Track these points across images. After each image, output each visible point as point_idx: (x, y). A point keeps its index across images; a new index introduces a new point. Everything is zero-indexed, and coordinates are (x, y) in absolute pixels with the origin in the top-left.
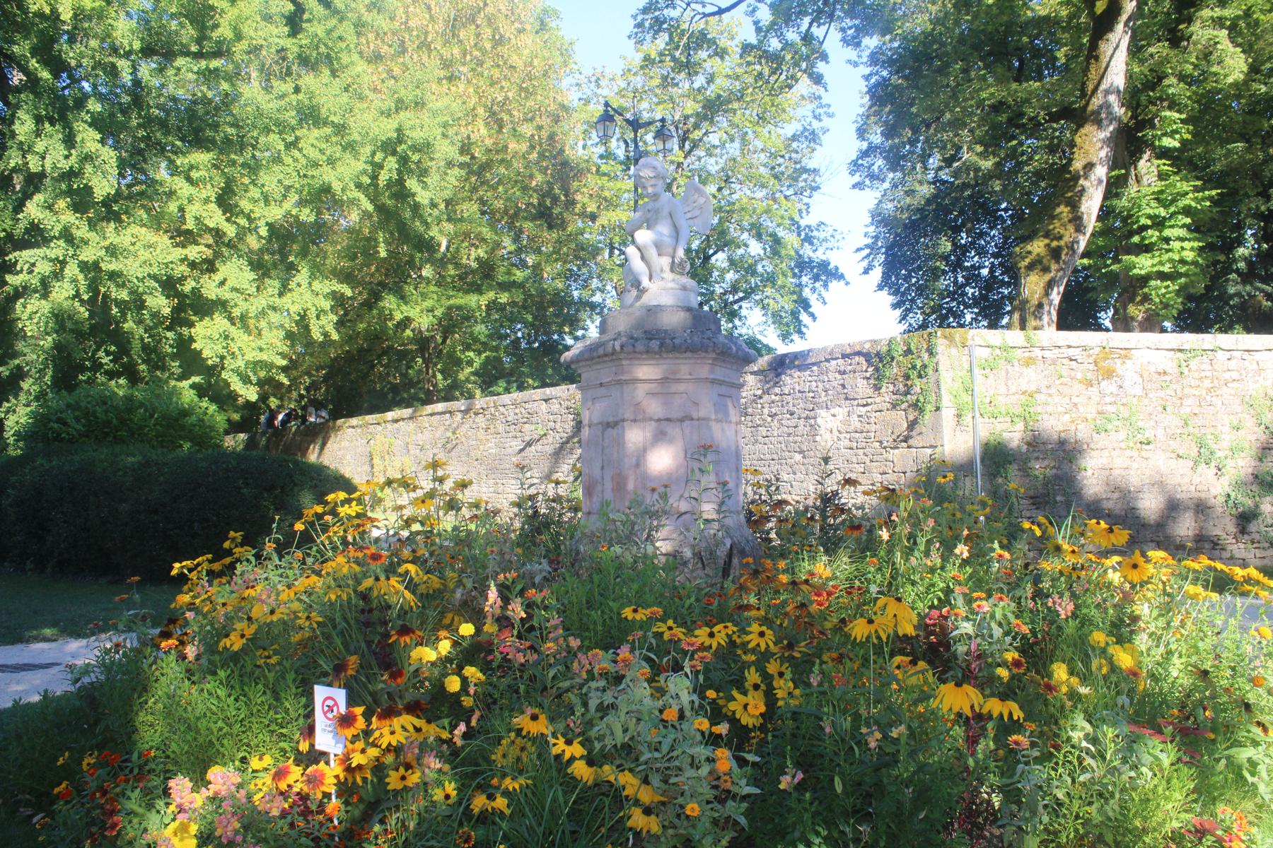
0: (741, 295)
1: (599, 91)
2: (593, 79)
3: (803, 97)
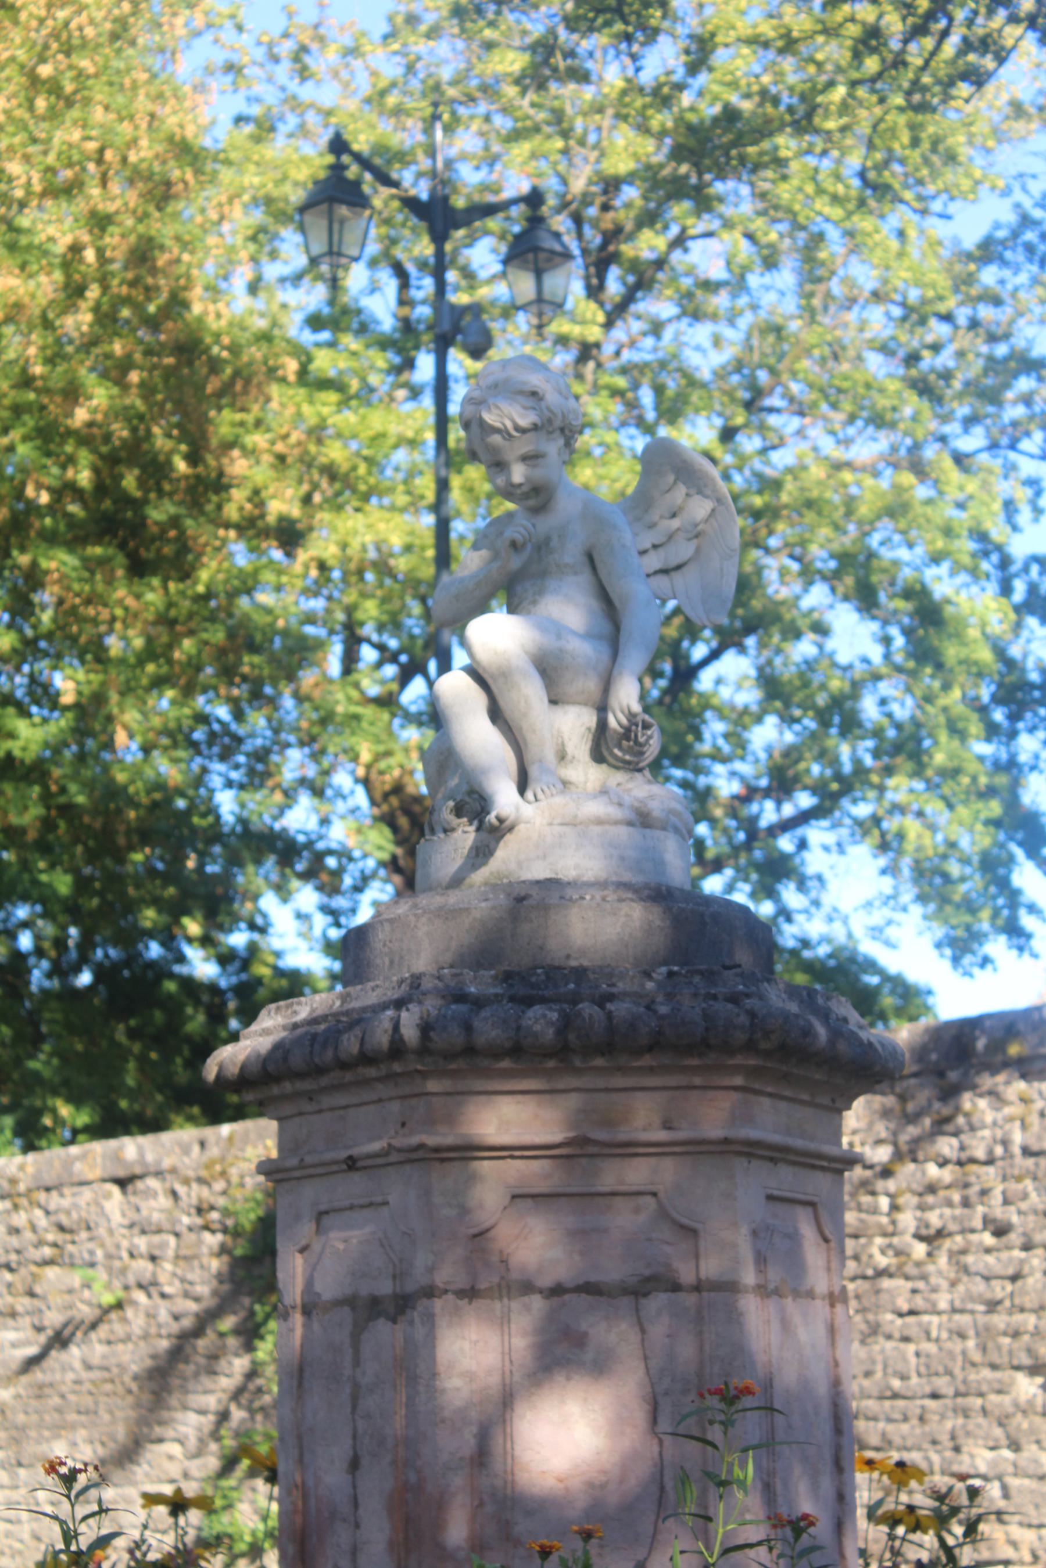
0: (805, 800)
1: (306, 92)
2: (286, 48)
3: (1018, 109)
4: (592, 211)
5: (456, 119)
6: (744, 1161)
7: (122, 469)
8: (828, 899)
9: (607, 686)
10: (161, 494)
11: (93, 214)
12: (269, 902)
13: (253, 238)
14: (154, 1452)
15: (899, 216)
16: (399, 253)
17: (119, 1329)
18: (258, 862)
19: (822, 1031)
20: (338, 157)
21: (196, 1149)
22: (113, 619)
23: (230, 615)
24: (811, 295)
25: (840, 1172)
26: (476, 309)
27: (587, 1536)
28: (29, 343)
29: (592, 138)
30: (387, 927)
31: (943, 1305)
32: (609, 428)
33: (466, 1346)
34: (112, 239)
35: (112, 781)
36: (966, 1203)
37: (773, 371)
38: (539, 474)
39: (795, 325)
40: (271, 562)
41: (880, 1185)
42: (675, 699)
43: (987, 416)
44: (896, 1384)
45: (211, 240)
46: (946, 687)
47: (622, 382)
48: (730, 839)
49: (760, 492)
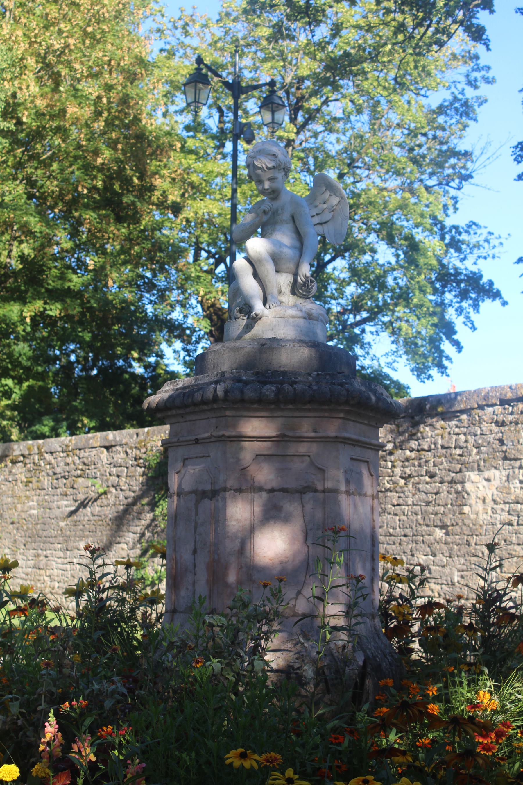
0: (365, 315)
1: (187, 41)
2: (180, 24)
3: (454, 56)
4: (293, 90)
5: (243, 53)
6: (343, 445)
7: (114, 182)
8: (372, 352)
9: (298, 266)
10: (128, 191)
11: (106, 84)
12: (164, 346)
13: (165, 96)
14: (116, 547)
15: (409, 95)
16: (220, 103)
17: (105, 502)
18: (161, 331)
19: (373, 398)
20: (199, 66)
21: (135, 436)
22: (109, 238)
23: (153, 238)
24: (374, 124)
25: (378, 450)
26: (249, 125)
27: (281, 580)
28: (81, 133)
29: (294, 62)
30: (213, 354)
31: (410, 502)
32: (297, 172)
33: (238, 510)
34: (113, 94)
35: (107, 298)
36: (420, 465)
37: (358, 152)
38: (275, 185)
39: (368, 135)
40: (169, 218)
41: (388, 458)
42: (318, 275)
43: (438, 173)
44: (391, 531)
45: (150, 96)
46: (419, 274)
47: (302, 155)
48: (336, 328)
49: (352, 198)
